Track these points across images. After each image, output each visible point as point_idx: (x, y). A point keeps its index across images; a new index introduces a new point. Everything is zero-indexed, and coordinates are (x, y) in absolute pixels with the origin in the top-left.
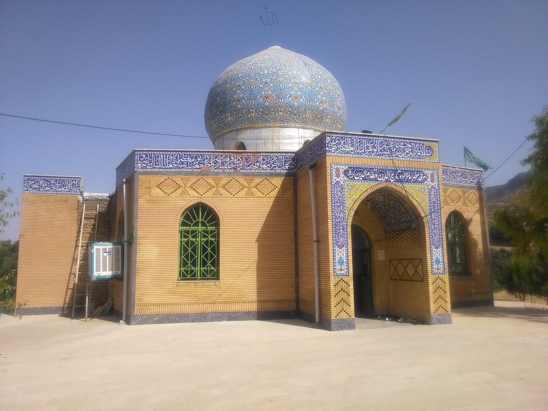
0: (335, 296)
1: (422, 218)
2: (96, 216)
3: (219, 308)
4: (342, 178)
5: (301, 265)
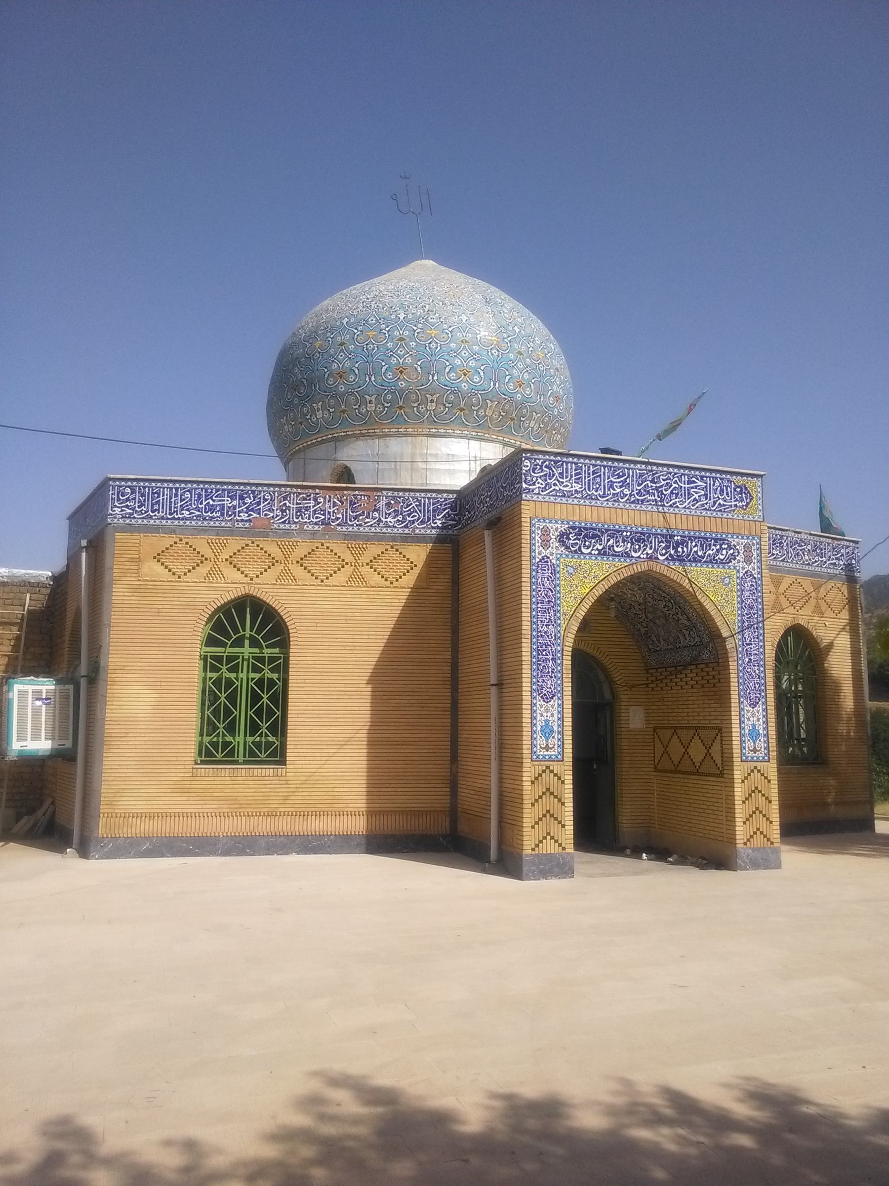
0: (533, 805)
1: (724, 640)
2: (22, 619)
3: (284, 825)
4: (555, 550)
5: (464, 735)
